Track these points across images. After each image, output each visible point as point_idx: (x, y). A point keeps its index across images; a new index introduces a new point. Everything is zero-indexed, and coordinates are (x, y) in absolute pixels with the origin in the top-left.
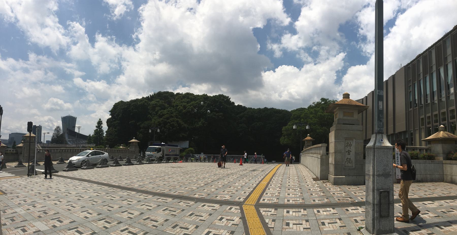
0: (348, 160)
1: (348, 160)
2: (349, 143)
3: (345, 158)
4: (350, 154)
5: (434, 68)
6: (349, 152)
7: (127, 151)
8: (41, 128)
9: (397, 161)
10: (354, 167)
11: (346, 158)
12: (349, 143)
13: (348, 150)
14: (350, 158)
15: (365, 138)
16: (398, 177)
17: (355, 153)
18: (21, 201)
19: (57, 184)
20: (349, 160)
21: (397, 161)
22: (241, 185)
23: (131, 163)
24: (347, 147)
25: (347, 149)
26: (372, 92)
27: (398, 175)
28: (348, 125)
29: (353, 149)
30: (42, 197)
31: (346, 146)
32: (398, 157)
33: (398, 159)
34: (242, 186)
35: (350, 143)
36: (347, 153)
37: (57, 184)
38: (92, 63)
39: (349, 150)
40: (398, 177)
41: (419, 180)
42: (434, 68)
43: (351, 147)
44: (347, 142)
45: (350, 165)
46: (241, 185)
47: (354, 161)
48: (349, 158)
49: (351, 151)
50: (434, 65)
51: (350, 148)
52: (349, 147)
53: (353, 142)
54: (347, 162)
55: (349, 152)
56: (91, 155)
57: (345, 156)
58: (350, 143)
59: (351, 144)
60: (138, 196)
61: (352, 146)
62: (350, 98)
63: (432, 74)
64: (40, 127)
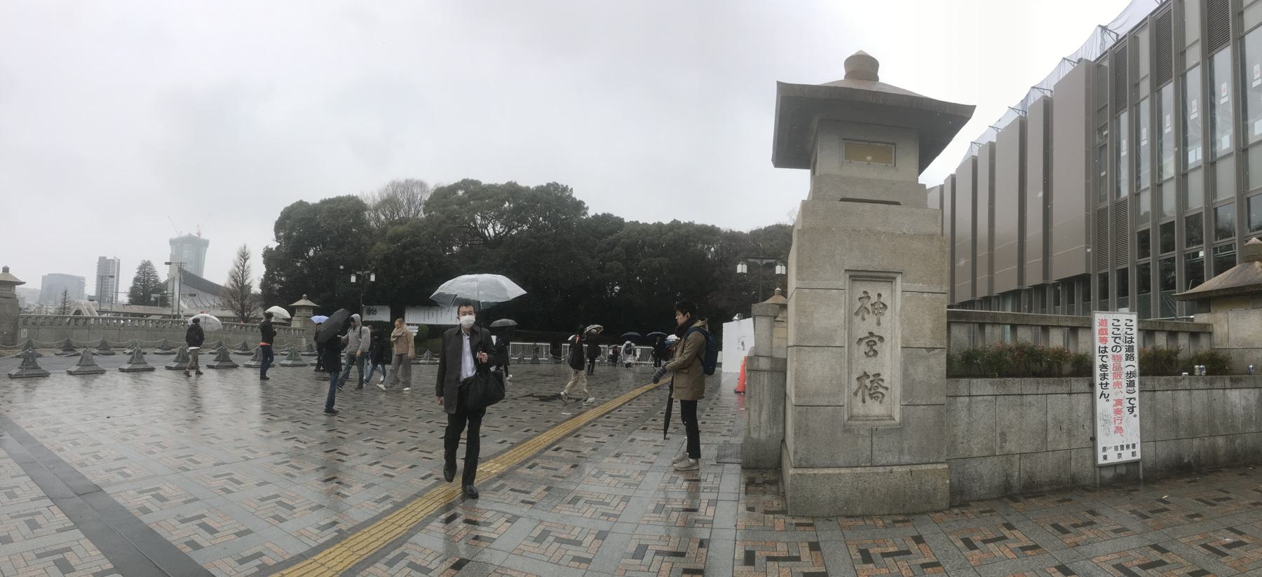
0: (867, 382)
1: (867, 382)
2: (874, 299)
3: (849, 374)
4: (876, 353)
5: (1145, 88)
6: (872, 343)
7: (244, 327)
8: (119, 264)
9: (1101, 384)
10: (897, 418)
11: (855, 376)
12: (874, 299)
13: (867, 335)
14: (879, 375)
15: (970, 294)
16: (1105, 457)
17: (902, 347)
18: (84, 457)
19: (177, 410)
20: (872, 386)
21: (1101, 384)
22: (622, 421)
23: (231, 361)
24: (859, 318)
25: (865, 326)
26: (971, 160)
27: (1104, 449)
28: (868, 206)
29: (892, 327)
30: (142, 444)
31: (857, 314)
32: (1104, 366)
33: (1104, 376)
34: (637, 415)
35: (879, 295)
36: (864, 347)
37: (177, 410)
38: (726, 232)
39: (871, 334)
40: (1105, 457)
41: (1186, 461)
42: (1145, 88)
43: (882, 319)
44: (861, 294)
45: (876, 409)
46: (622, 421)
47: (897, 391)
48: (871, 372)
49: (881, 339)
50: (1143, 79)
51: (879, 324)
52: (871, 320)
53: (893, 291)
54: (860, 393)
55: (871, 344)
56: (511, 322)
57: (850, 363)
58: (879, 295)
59: (882, 300)
60: (361, 442)
61: (888, 313)
62: (929, 207)
63: (1138, 105)
64: (116, 261)
